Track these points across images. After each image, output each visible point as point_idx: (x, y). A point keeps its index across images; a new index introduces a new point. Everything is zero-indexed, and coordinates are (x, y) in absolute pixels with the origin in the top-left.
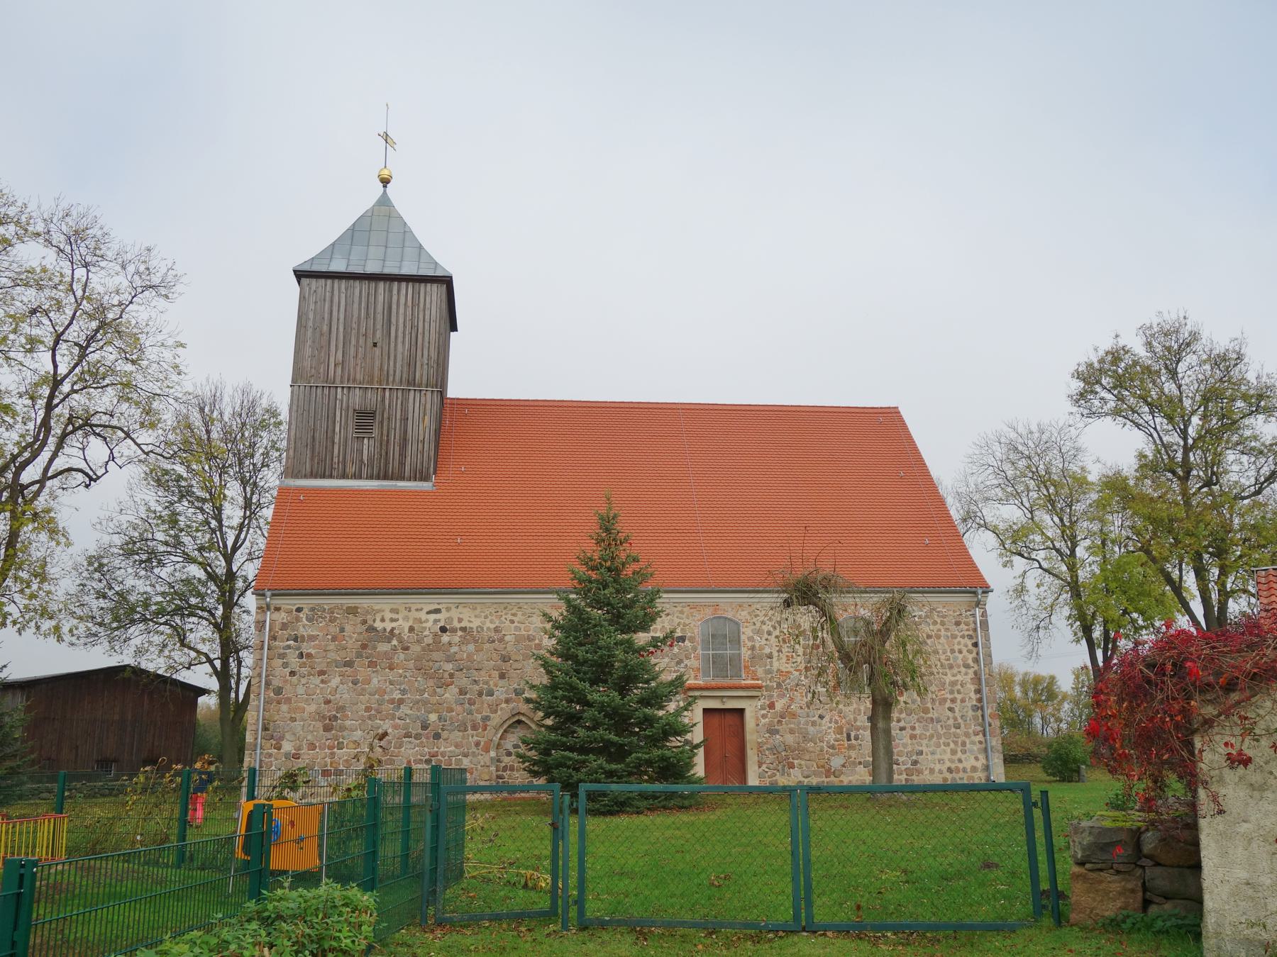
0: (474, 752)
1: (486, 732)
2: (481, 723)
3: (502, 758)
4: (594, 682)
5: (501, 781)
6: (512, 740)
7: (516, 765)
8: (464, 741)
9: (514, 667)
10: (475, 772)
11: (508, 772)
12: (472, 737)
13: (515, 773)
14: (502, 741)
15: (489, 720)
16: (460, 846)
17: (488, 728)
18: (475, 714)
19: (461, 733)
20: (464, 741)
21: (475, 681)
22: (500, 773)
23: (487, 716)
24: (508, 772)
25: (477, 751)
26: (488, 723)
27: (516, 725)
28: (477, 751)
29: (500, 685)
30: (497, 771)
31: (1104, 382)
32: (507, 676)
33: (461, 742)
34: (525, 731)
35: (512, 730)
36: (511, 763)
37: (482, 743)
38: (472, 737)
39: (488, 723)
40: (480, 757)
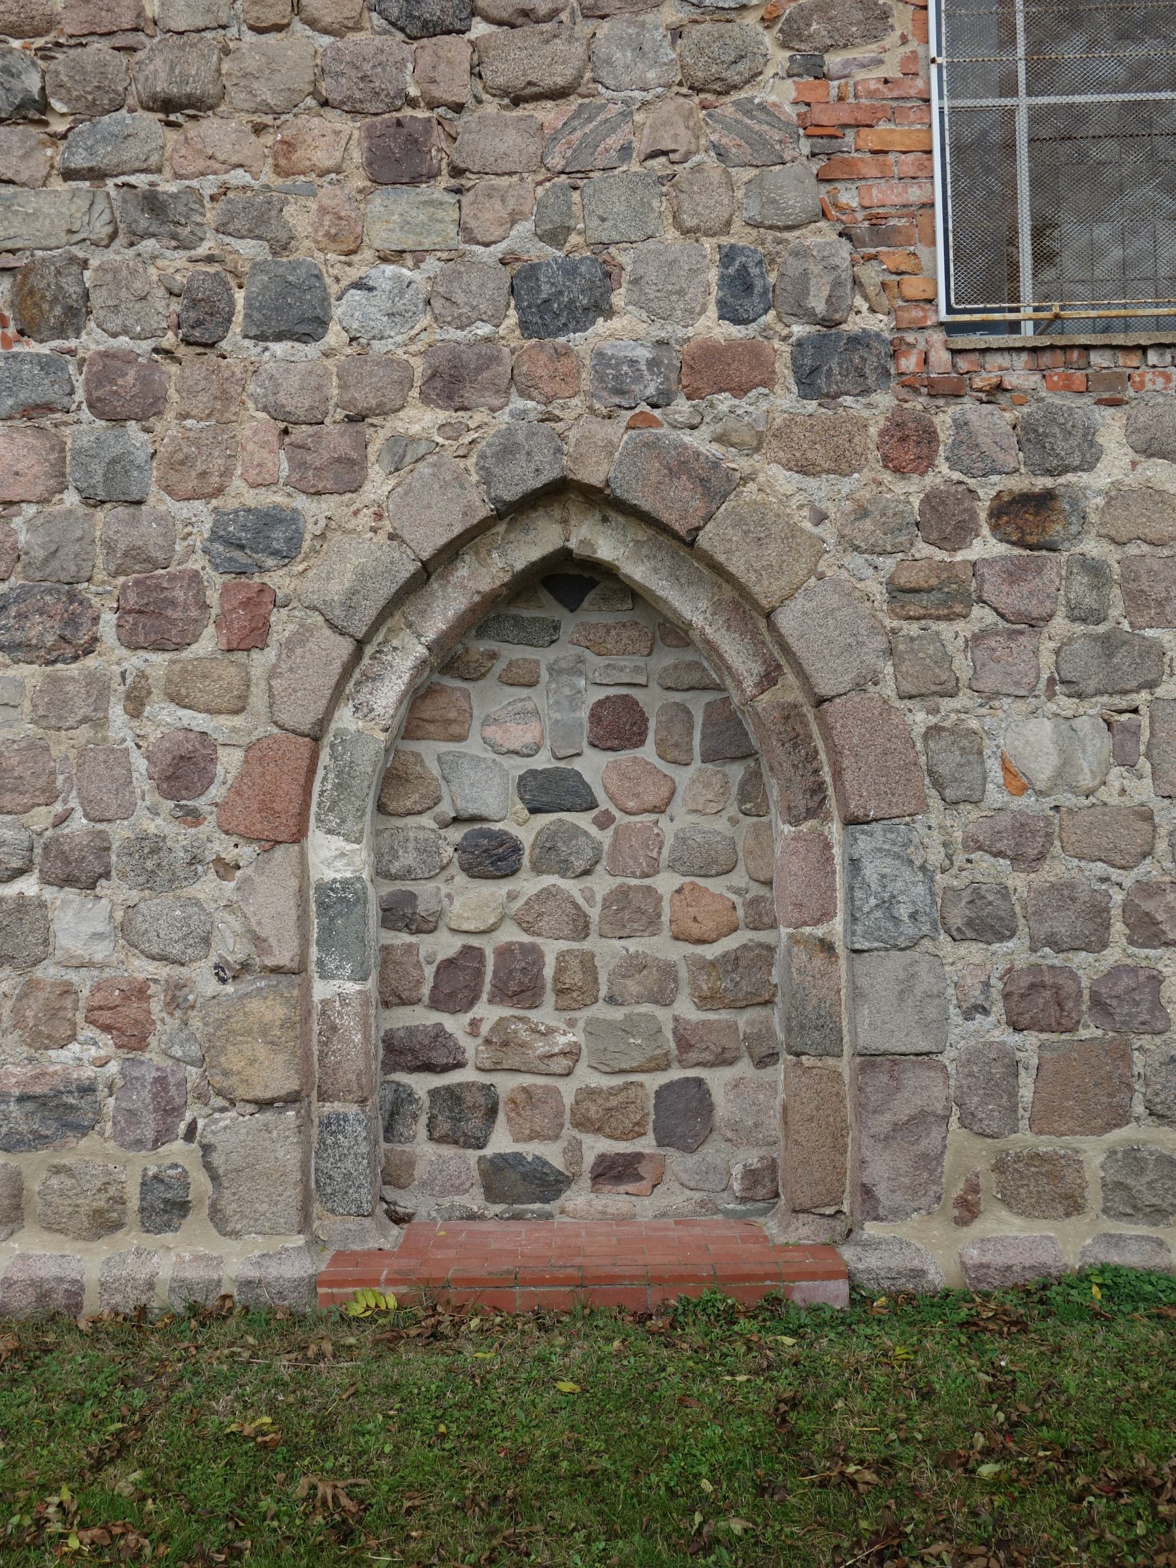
0: (156, 846)
1: (261, 661)
2: (215, 583)
3: (426, 892)
4: (947, 459)
5: (422, 1084)
6: (521, 734)
7: (551, 949)
8: (62, 746)
9: (502, 72)
10: (165, 1025)
11: (488, 1012)
12: (136, 703)
13: (545, 1015)
14: (430, 751)
15: (287, 556)
16: (681, 616)
17: (282, 625)
18: (159, 502)
19: (31, 674)
20: (62, 746)
21: (153, 203)
22: (421, 1017)
23: (270, 519)
24: (488, 1012)
25: (179, 836)
26: (280, 580)
27: (550, 609)
28: (179, 836)
29: (382, 236)
30: (391, 998)
31: (193, 1072)
32: (439, 151)
33: (37, 748)
34: (627, 666)
35: (513, 653)
36: (511, 934)
37: (229, 762)
38: (136, 703)
39: (280, 580)
40: (207, 888)
